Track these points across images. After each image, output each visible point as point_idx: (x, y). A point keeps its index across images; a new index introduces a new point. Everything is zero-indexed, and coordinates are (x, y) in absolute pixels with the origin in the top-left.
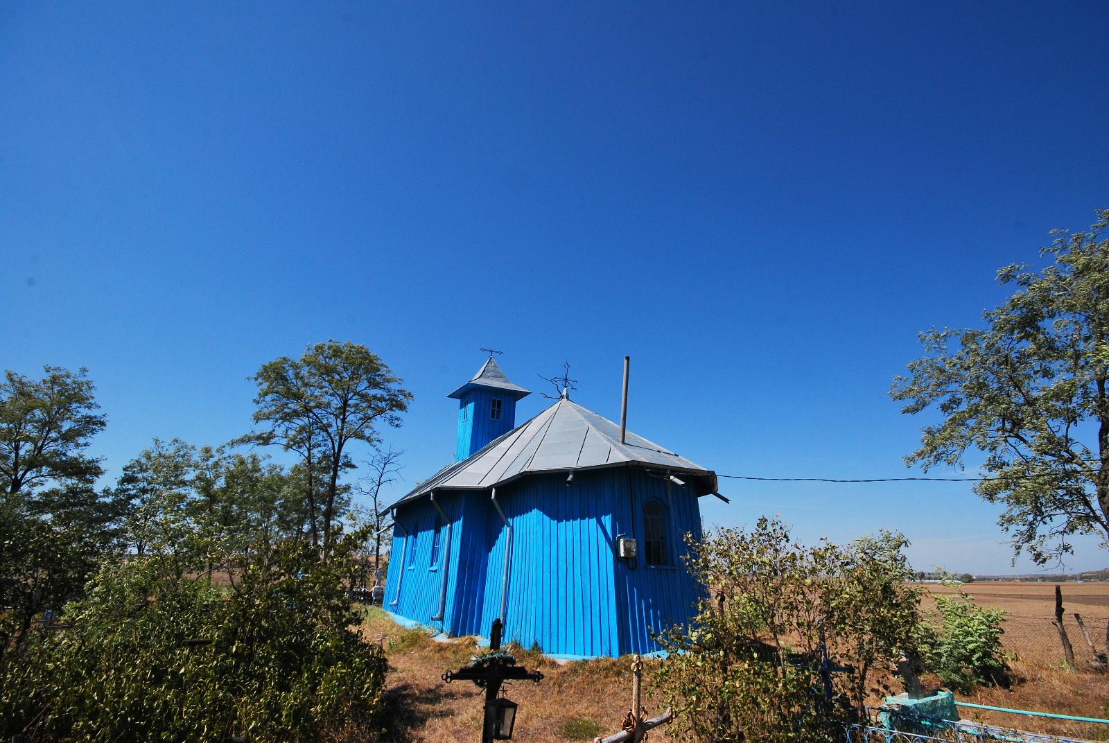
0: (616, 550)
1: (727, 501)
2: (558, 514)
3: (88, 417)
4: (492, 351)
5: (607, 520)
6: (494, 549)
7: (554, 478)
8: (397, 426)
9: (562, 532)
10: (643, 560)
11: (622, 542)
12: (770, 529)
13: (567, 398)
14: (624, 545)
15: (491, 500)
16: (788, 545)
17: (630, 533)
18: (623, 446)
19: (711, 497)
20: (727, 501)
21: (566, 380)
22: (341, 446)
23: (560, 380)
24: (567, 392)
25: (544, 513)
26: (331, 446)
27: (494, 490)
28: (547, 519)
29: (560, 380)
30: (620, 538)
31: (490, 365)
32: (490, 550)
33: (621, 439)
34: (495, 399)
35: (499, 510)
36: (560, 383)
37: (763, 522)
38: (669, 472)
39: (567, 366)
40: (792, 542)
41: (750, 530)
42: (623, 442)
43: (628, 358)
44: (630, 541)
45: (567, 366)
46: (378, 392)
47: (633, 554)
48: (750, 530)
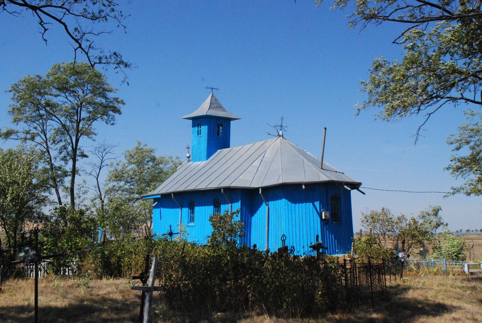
0: (321, 217)
1: (364, 194)
2: (294, 200)
3: (62, 147)
4: (212, 89)
5: (317, 204)
6: (256, 215)
7: (296, 186)
8: (112, 124)
9: (200, 209)
10: (330, 220)
11: (323, 213)
12: (385, 211)
13: (282, 136)
14: (324, 214)
15: (259, 194)
16: (390, 215)
17: (326, 210)
18: (322, 170)
19: (356, 190)
20: (364, 194)
21: (281, 126)
22: (77, 141)
23: (278, 126)
24: (282, 133)
25: (288, 200)
26: (69, 141)
27: (260, 190)
28: (290, 203)
29: (278, 126)
30: (322, 211)
31: (212, 99)
32: (252, 215)
33: (321, 167)
34: (219, 123)
35: (263, 198)
36: (279, 128)
37: (383, 209)
38: (344, 184)
39: (282, 118)
40: (391, 214)
41: (380, 211)
42: (322, 169)
43: (325, 129)
44: (327, 212)
45: (282, 118)
46: (99, 100)
47: (328, 218)
48: (380, 211)
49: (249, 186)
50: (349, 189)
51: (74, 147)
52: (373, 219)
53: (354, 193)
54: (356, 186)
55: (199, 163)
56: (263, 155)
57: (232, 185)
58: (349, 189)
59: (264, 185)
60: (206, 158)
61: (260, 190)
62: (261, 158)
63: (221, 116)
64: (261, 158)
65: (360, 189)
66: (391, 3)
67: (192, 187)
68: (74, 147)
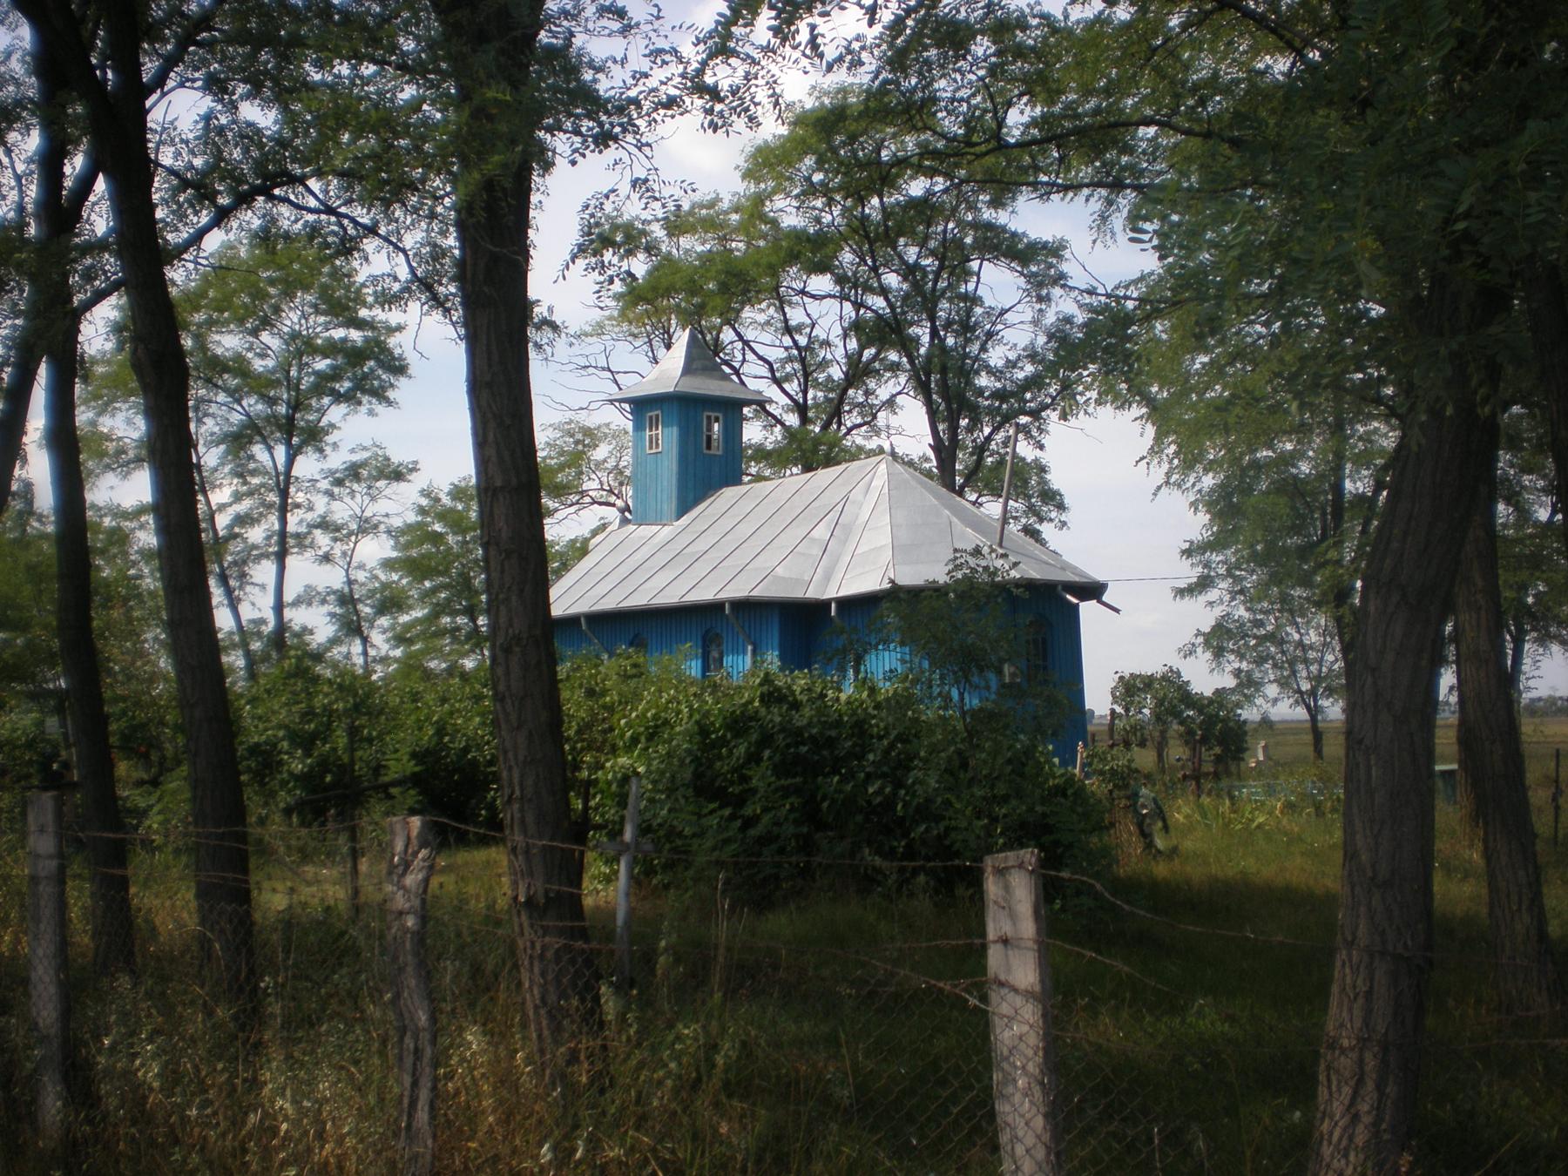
1: (1117, 611)
20: (1117, 611)
38: (1060, 588)
49: (800, 595)
50: (1075, 601)
51: (43, 372)
52: (1130, 688)
53: (1088, 611)
54: (1093, 591)
55: (655, 528)
56: (839, 508)
57: (755, 593)
58: (1075, 601)
59: (844, 592)
60: (669, 503)
61: (833, 605)
62: (834, 515)
63: (718, 393)
64: (834, 515)
65: (1105, 598)
66: (1555, 799)
67: (639, 600)
68: (43, 372)
